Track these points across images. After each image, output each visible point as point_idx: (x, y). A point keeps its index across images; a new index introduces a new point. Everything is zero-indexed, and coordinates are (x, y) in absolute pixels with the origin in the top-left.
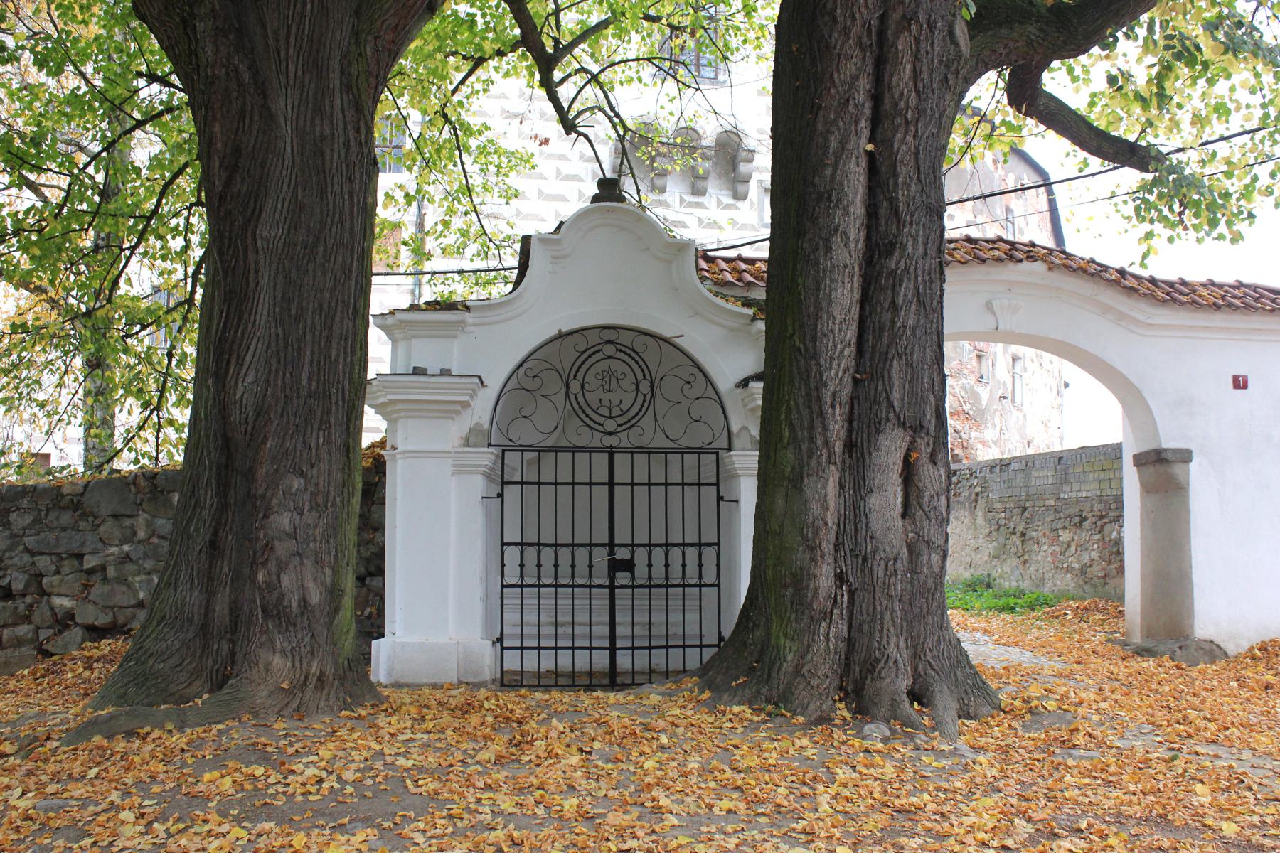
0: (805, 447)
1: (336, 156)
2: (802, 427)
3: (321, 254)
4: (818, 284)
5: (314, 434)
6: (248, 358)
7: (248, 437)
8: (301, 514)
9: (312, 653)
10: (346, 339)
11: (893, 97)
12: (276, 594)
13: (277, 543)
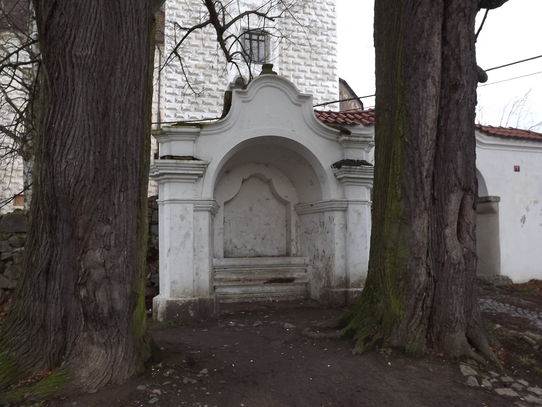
0: (412, 199)
3: (119, 70)
5: (117, 195)
6: (69, 142)
7: (71, 197)
8: (109, 250)
12: (93, 305)
13: (92, 271)
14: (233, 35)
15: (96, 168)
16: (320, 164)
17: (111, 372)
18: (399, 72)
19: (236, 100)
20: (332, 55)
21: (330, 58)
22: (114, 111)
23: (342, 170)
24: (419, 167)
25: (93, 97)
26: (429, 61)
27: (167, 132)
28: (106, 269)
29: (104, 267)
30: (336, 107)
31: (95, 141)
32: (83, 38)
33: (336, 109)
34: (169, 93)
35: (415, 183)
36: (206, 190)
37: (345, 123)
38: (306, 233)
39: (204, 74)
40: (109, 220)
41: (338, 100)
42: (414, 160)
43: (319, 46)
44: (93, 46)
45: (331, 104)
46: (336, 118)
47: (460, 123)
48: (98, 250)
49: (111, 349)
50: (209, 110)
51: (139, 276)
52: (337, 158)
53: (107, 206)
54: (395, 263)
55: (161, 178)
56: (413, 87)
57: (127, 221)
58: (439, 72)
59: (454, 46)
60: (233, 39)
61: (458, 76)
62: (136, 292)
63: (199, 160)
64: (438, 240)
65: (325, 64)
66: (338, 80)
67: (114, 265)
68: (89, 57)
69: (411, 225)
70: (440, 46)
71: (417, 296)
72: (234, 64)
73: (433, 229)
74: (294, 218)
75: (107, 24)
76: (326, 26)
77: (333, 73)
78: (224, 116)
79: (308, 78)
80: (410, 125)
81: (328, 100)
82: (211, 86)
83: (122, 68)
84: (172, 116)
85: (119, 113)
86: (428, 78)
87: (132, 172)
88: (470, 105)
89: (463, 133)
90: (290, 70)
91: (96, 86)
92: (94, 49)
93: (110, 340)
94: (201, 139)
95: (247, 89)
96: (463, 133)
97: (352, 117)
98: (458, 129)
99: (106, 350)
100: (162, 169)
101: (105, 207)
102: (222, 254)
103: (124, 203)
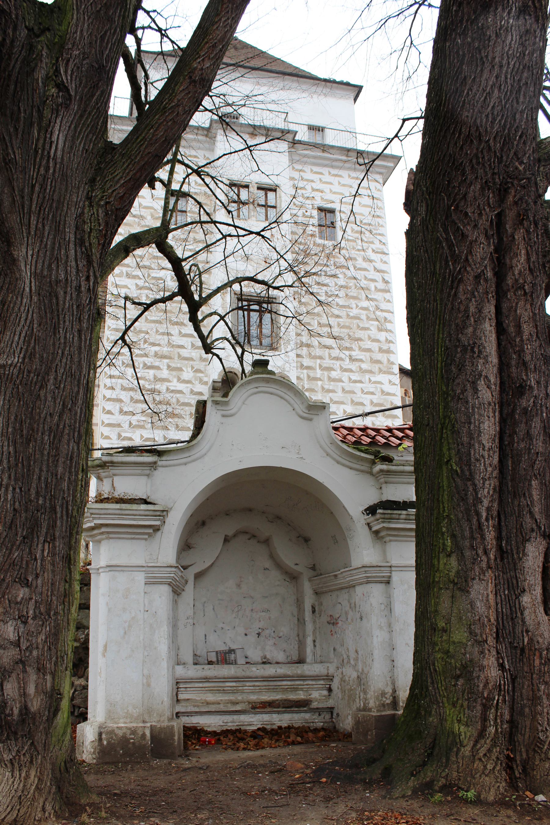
0: (468, 553)
1: (68, 298)
2: (463, 538)
3: (51, 381)
4: (469, 418)
5: (40, 546)
8: (25, 623)
9: (31, 762)
10: (71, 459)
11: (514, 275)
14: (215, 313)
15: (15, 510)
16: (344, 506)
17: (18, 807)
18: (439, 371)
19: (212, 416)
20: (387, 331)
21: (382, 336)
22: (42, 434)
23: (378, 516)
24: (474, 505)
25: (16, 416)
26: (479, 356)
27: (108, 462)
28: (20, 650)
29: (20, 647)
30: (396, 417)
31: (16, 473)
32: (10, 343)
33: (397, 420)
34: (109, 400)
35: (471, 528)
36: (166, 548)
37: (387, 445)
38: (329, 623)
39: (169, 367)
40: (28, 580)
41: (400, 404)
42: (466, 495)
43: (364, 317)
44: (20, 353)
45: (387, 413)
46: (373, 438)
47: (531, 439)
48: (10, 623)
49: (20, 770)
50: (177, 426)
51: (64, 666)
52: (372, 499)
53: (27, 561)
54: (448, 651)
55: (95, 532)
56: (458, 391)
57: (52, 584)
58: (495, 370)
59: (514, 334)
60: (216, 318)
61: (524, 374)
62: (59, 690)
63: (154, 504)
64: (511, 614)
65: (375, 346)
66: (397, 370)
67: (31, 645)
68: (16, 366)
69: (468, 592)
70: (494, 335)
71: (484, 701)
72: (215, 357)
73: (503, 596)
74: (309, 601)
75: (40, 325)
76: (372, 286)
77: (389, 360)
78: (194, 436)
79: (346, 370)
80: (458, 445)
81: (381, 405)
82: (181, 387)
83: (55, 379)
84: (114, 436)
85: (49, 436)
86: (479, 378)
87: (62, 516)
88: (544, 414)
89: (538, 453)
90: (315, 357)
91: (22, 403)
92: (22, 355)
93: (20, 756)
94: (160, 474)
95: (229, 397)
96: (538, 453)
97: (400, 434)
98: (529, 449)
99: (13, 771)
100: (99, 518)
101: (24, 562)
102: (189, 659)
103: (49, 558)
